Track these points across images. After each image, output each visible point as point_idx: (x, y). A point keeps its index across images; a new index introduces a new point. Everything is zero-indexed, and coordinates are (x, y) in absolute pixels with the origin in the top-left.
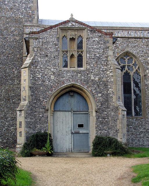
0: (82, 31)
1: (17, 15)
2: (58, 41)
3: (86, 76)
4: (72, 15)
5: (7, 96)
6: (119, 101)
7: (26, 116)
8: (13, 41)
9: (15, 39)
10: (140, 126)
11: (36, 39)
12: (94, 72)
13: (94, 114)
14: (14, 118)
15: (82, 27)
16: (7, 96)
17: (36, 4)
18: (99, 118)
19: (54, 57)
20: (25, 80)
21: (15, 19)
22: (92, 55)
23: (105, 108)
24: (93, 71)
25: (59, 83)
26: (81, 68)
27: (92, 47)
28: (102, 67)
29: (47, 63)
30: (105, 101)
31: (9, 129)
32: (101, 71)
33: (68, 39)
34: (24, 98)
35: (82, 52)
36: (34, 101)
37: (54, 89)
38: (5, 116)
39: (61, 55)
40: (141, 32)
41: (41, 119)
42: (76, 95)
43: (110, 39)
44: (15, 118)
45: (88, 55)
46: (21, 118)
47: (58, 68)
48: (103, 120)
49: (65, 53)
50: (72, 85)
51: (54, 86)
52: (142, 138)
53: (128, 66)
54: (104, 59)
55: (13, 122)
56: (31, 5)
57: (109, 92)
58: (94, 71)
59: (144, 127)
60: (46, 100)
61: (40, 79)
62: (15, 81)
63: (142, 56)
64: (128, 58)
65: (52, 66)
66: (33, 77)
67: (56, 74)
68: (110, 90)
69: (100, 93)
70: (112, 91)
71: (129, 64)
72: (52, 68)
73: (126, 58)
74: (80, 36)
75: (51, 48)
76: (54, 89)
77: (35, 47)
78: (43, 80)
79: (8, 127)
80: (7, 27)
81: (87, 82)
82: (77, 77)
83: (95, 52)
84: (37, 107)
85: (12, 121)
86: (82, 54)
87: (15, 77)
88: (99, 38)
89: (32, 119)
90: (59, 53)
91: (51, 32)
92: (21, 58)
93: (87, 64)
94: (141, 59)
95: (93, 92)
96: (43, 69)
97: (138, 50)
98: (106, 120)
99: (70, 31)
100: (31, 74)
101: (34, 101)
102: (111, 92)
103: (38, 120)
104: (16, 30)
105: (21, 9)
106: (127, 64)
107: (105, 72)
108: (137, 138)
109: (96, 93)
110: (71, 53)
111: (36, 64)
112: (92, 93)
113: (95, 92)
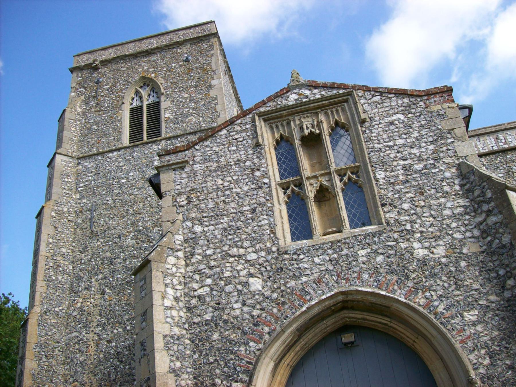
11: (183, 168)
25: (284, 303)
28: (449, 205)
29: (230, 237)
37: (267, 329)
50: (340, 298)
61: (208, 299)
69: (470, 306)
72: (250, 250)
77: (179, 194)
93: (383, 205)
96: (215, 260)
100: (166, 285)
109: (453, 311)
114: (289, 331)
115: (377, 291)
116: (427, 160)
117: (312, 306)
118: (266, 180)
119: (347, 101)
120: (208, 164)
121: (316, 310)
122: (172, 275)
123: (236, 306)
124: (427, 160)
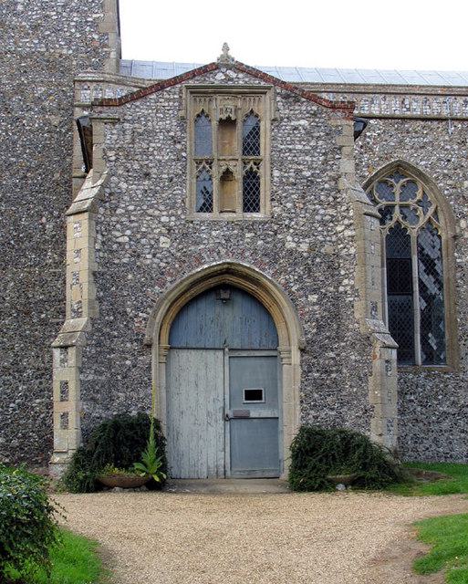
0: (257, 98)
1: (54, 48)
2: (183, 130)
3: (269, 240)
4: (226, 47)
5: (22, 300)
6: (373, 317)
7: (83, 363)
8: (41, 128)
9: (47, 123)
10: (440, 397)
11: (114, 124)
12: (295, 226)
13: (296, 357)
14: (43, 371)
15: (259, 83)
16: (22, 300)
17: (112, 14)
18: (310, 372)
19: (171, 180)
20: (79, 251)
21: (48, 61)
22: (290, 174)
23: (328, 338)
24: (293, 223)
25: (184, 262)
26: (254, 215)
27: (290, 147)
28: (322, 212)
29: (149, 199)
30: (329, 318)
31: (29, 404)
32: (319, 222)
33: (215, 123)
34: (75, 307)
35: (257, 162)
36: (107, 318)
37: (169, 279)
38: (15, 363)
39: (191, 174)
40: (441, 99)
41: (130, 374)
42: (238, 299)
43: (345, 122)
44: (46, 369)
45: (276, 173)
46: (65, 370)
47: (183, 213)
48: (323, 376)
49: (204, 167)
50: (226, 266)
51: (171, 271)
52: (446, 434)
53: (401, 206)
54: (327, 186)
55: (41, 383)
56: (98, 15)
57: (341, 289)
58: (297, 224)
59: (452, 398)
60: (145, 315)
61: (127, 247)
62: (46, 255)
63: (445, 175)
64: (402, 181)
65: (162, 208)
66: (103, 242)
67: (177, 231)
68: (346, 281)
69: (314, 291)
70: (352, 287)
71: (405, 201)
72: (165, 213)
73: (397, 183)
74: (252, 112)
75: (160, 149)
76: (169, 279)
77: (111, 149)
78: (135, 252)
79: (26, 398)
80: (23, 83)
81: (273, 256)
82: (241, 242)
83: (299, 164)
84: (115, 337)
85: (39, 380)
86: (258, 168)
87: (46, 241)
88: (312, 120)
89: (101, 373)
90: (185, 167)
91: (161, 100)
92: (66, 183)
93: (272, 200)
94: (442, 185)
95: (293, 289)
96: (135, 216)
97: (434, 158)
98: (333, 375)
99: (219, 98)
100: (97, 232)
101: (107, 318)
102: (348, 288)
103: (119, 378)
104: (50, 95)
105: (66, 29)
106: (400, 201)
107: (331, 224)
108: (430, 434)
109: (301, 292)
110: (224, 168)
111: (113, 202)
112: (290, 292)
113: (298, 290)
114: (185, 283)
115: (253, 267)
116: (315, 169)
117: (184, 280)
118: (184, 154)
119: (265, 93)
120: (137, 125)
121: (200, 275)
122: (102, 223)
123: (148, 256)
124: (315, 169)
